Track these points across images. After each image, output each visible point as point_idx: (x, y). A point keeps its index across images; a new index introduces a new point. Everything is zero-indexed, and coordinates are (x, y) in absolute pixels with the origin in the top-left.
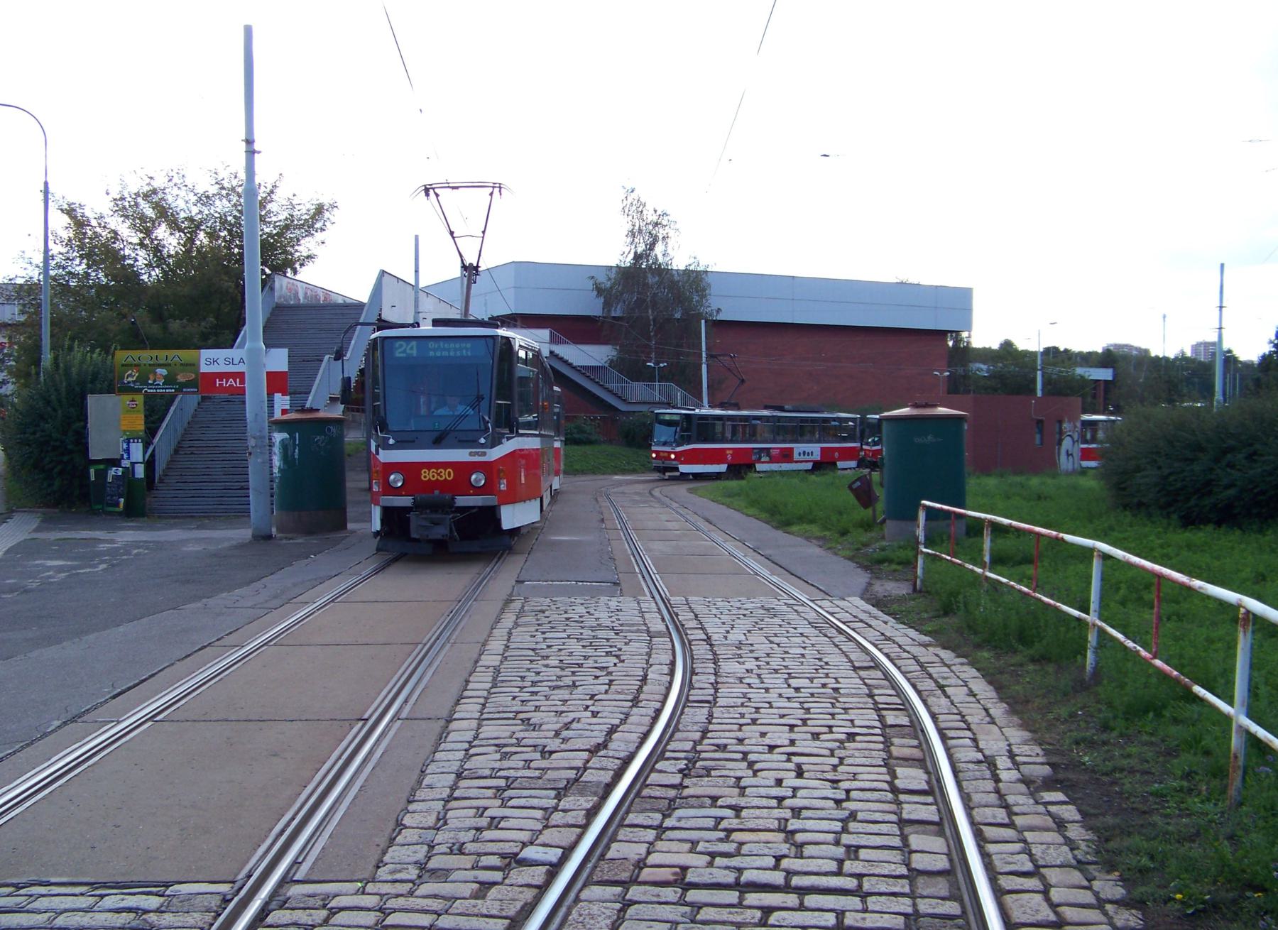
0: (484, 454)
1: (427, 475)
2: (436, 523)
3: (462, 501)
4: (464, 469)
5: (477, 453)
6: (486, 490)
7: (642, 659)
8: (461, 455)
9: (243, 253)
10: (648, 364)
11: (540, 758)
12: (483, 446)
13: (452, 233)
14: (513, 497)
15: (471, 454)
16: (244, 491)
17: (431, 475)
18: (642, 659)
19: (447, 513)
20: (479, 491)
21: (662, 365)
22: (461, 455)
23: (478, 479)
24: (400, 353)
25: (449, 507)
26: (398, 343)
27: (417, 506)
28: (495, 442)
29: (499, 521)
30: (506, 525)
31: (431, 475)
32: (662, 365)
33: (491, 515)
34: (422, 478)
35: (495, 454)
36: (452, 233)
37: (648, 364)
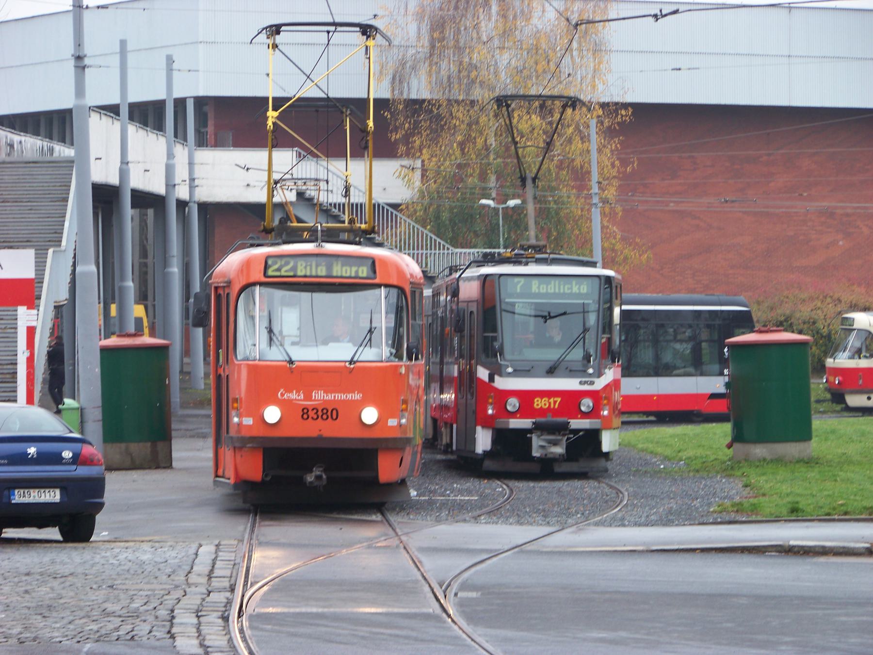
0: (592, 383)
1: (540, 403)
2: (555, 443)
3: (576, 423)
4: (571, 399)
5: (585, 383)
6: (593, 413)
7: (207, 607)
9: (485, 330)
10: (484, 201)
11: (59, 537)
12: (590, 375)
15: (581, 383)
16: (57, 235)
17: (543, 403)
18: (207, 607)
19: (564, 435)
20: (585, 415)
21: (512, 203)
24: (273, 271)
25: (562, 429)
27: (538, 428)
29: (599, 443)
31: (543, 403)
33: (593, 436)
34: (535, 405)
37: (484, 201)
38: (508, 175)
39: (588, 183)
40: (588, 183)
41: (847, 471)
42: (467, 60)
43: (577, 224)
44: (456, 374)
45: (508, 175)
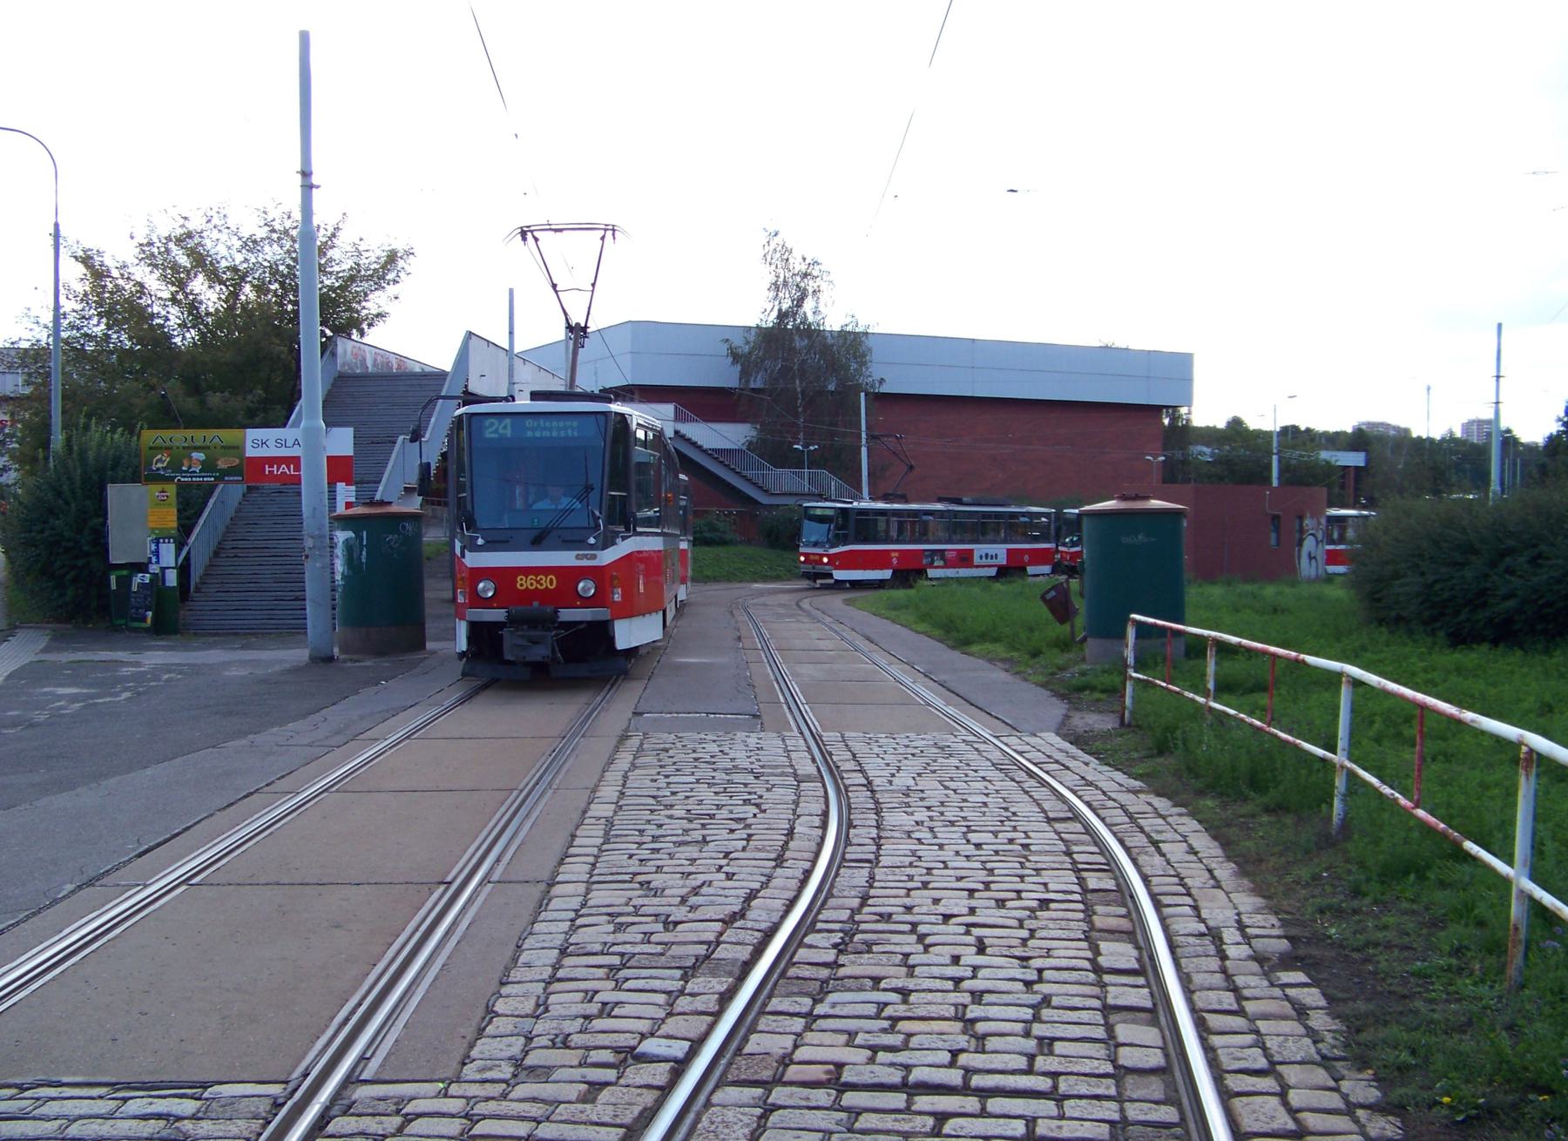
0: (594, 557)
1: (523, 583)
2: (535, 642)
3: (566, 615)
4: (569, 576)
5: (585, 556)
6: (596, 601)
8: (566, 558)
10: (795, 446)
12: (592, 547)
13: (554, 286)
14: (629, 610)
15: (577, 557)
17: (529, 582)
19: (549, 630)
20: (588, 602)
21: (812, 448)
22: (566, 558)
23: (586, 587)
25: (551, 622)
26: (488, 421)
27: (512, 621)
28: (607, 542)
29: (612, 639)
30: (621, 644)
31: (529, 582)
32: (812, 448)
33: (602, 632)
34: (518, 586)
35: (607, 557)
36: (554, 286)
37: (795, 446)
38: (53, 529)
39: (1509, 827)
40: (1509, 827)
41: (1261, 753)
42: (175, 333)
43: (822, 991)
44: (506, 517)
45: (53, 529)
